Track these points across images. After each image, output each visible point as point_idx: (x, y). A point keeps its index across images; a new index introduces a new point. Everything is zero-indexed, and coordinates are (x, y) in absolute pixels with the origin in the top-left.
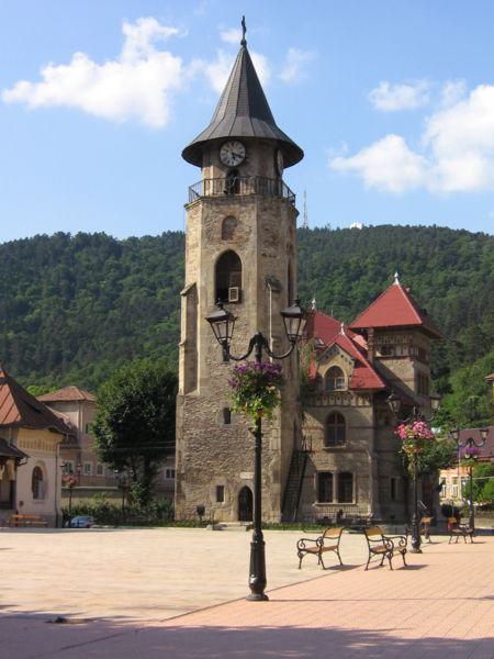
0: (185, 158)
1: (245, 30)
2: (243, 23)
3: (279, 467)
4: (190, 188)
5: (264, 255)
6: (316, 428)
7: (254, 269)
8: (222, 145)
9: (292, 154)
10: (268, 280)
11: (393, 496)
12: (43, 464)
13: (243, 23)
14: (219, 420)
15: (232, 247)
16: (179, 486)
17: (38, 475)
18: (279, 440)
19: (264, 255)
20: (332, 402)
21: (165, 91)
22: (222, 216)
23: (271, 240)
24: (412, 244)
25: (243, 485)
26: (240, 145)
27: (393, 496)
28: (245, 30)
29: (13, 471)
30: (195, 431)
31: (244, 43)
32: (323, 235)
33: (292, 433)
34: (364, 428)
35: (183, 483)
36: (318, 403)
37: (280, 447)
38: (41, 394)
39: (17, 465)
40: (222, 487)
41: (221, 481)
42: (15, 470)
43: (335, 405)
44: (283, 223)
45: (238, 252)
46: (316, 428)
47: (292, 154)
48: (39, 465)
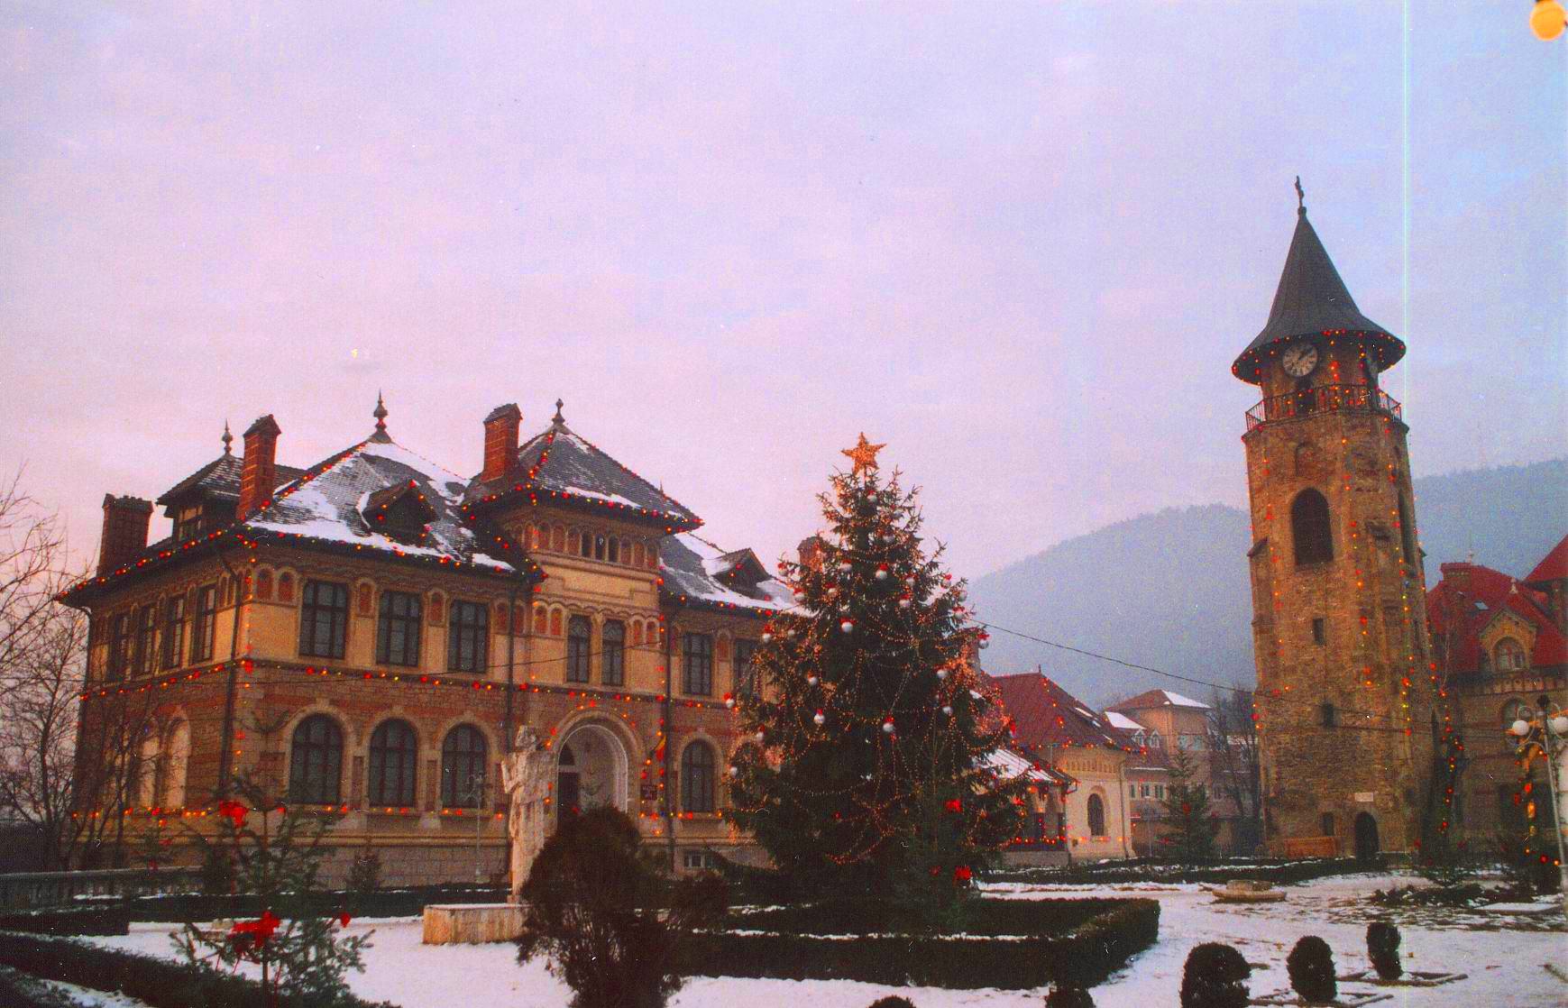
0: (508, 406)
1: (1301, 195)
2: (1298, 186)
4: (1247, 413)
5: (1359, 490)
9: (1390, 350)
10: (1370, 527)
12: (1102, 790)
13: (1298, 186)
15: (1312, 484)
17: (1096, 809)
19: (1359, 490)
20: (1508, 688)
28: (1301, 195)
29: (1060, 803)
30: (1284, 738)
31: (1302, 211)
32: (279, 466)
34: (596, 654)
35: (1274, 811)
36: (1487, 691)
39: (1064, 793)
42: (1063, 801)
43: (1513, 691)
44: (1383, 444)
45: (1321, 489)
47: (1390, 350)
48: (1096, 792)
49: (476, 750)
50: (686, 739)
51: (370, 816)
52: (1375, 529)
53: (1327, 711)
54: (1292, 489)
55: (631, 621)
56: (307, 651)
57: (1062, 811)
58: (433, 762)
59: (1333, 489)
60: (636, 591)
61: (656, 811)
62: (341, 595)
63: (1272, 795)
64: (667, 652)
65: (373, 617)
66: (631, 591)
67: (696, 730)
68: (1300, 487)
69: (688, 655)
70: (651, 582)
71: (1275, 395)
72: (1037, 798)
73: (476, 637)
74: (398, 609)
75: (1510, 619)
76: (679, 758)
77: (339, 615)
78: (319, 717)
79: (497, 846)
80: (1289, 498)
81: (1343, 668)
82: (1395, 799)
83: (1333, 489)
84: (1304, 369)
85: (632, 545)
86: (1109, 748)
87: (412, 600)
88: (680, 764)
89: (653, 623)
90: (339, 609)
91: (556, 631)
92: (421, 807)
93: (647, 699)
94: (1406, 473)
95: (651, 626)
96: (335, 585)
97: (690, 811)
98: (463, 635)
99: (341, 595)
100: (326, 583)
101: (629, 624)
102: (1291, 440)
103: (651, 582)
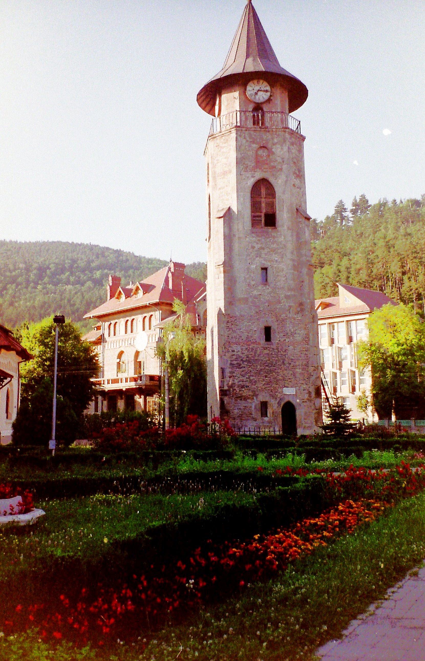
45: (272, 180)
54: (253, 177)
63: (226, 388)
68: (259, 175)
80: (251, 182)
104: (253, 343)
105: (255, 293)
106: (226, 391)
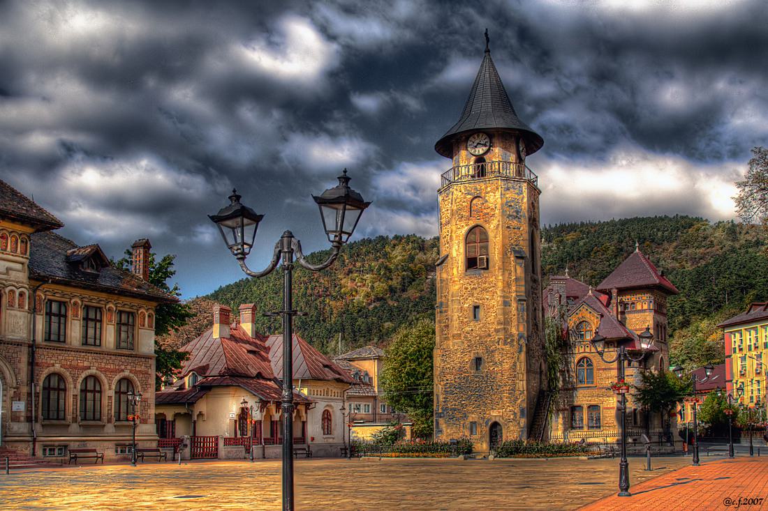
3: (525, 405)
4: (442, 176)
5: (508, 227)
6: (679, 441)
7: (499, 238)
8: (471, 136)
11: (635, 423)
14: (471, 368)
15: (480, 222)
16: (437, 423)
17: (327, 417)
18: (525, 382)
19: (508, 227)
21: (452, 158)
22: (469, 196)
23: (515, 214)
24: (658, 230)
25: (494, 420)
26: (485, 136)
27: (635, 423)
29: (304, 414)
33: (538, 376)
35: (441, 421)
37: (525, 389)
38: (183, 344)
39: (307, 409)
40: (765, 348)
41: (473, 417)
42: (306, 413)
45: (486, 226)
46: (679, 441)
49: (60, 387)
50: (45, 372)
51: (43, 426)
52: (515, 252)
53: (478, 361)
55: (7, 290)
56: (47, 338)
57: (305, 420)
58: (110, 397)
59: (492, 226)
60: (11, 269)
61: (22, 419)
62: (131, 318)
63: (440, 411)
64: (33, 311)
65: (42, 315)
66: (7, 269)
67: (53, 366)
69: (49, 314)
70: (23, 264)
71: (461, 165)
72: (177, 411)
73: (96, 326)
74: (92, 315)
75: (587, 310)
76: (41, 383)
77: (62, 316)
78: (54, 374)
79: (28, 441)
81: (489, 335)
82: (515, 414)
83: (492, 226)
84: (480, 150)
85: (9, 238)
86: (338, 382)
87: (98, 310)
88: (41, 388)
89: (25, 293)
90: (62, 316)
91: (21, 306)
92: (106, 421)
93: (19, 344)
94: (537, 219)
95: (21, 294)
96: (96, 308)
97: (48, 419)
98: (89, 325)
99: (131, 318)
100: (56, 301)
101: (5, 292)
102: (469, 194)
103: (23, 264)
104: (465, 372)
105: (468, 329)
106: (441, 413)
